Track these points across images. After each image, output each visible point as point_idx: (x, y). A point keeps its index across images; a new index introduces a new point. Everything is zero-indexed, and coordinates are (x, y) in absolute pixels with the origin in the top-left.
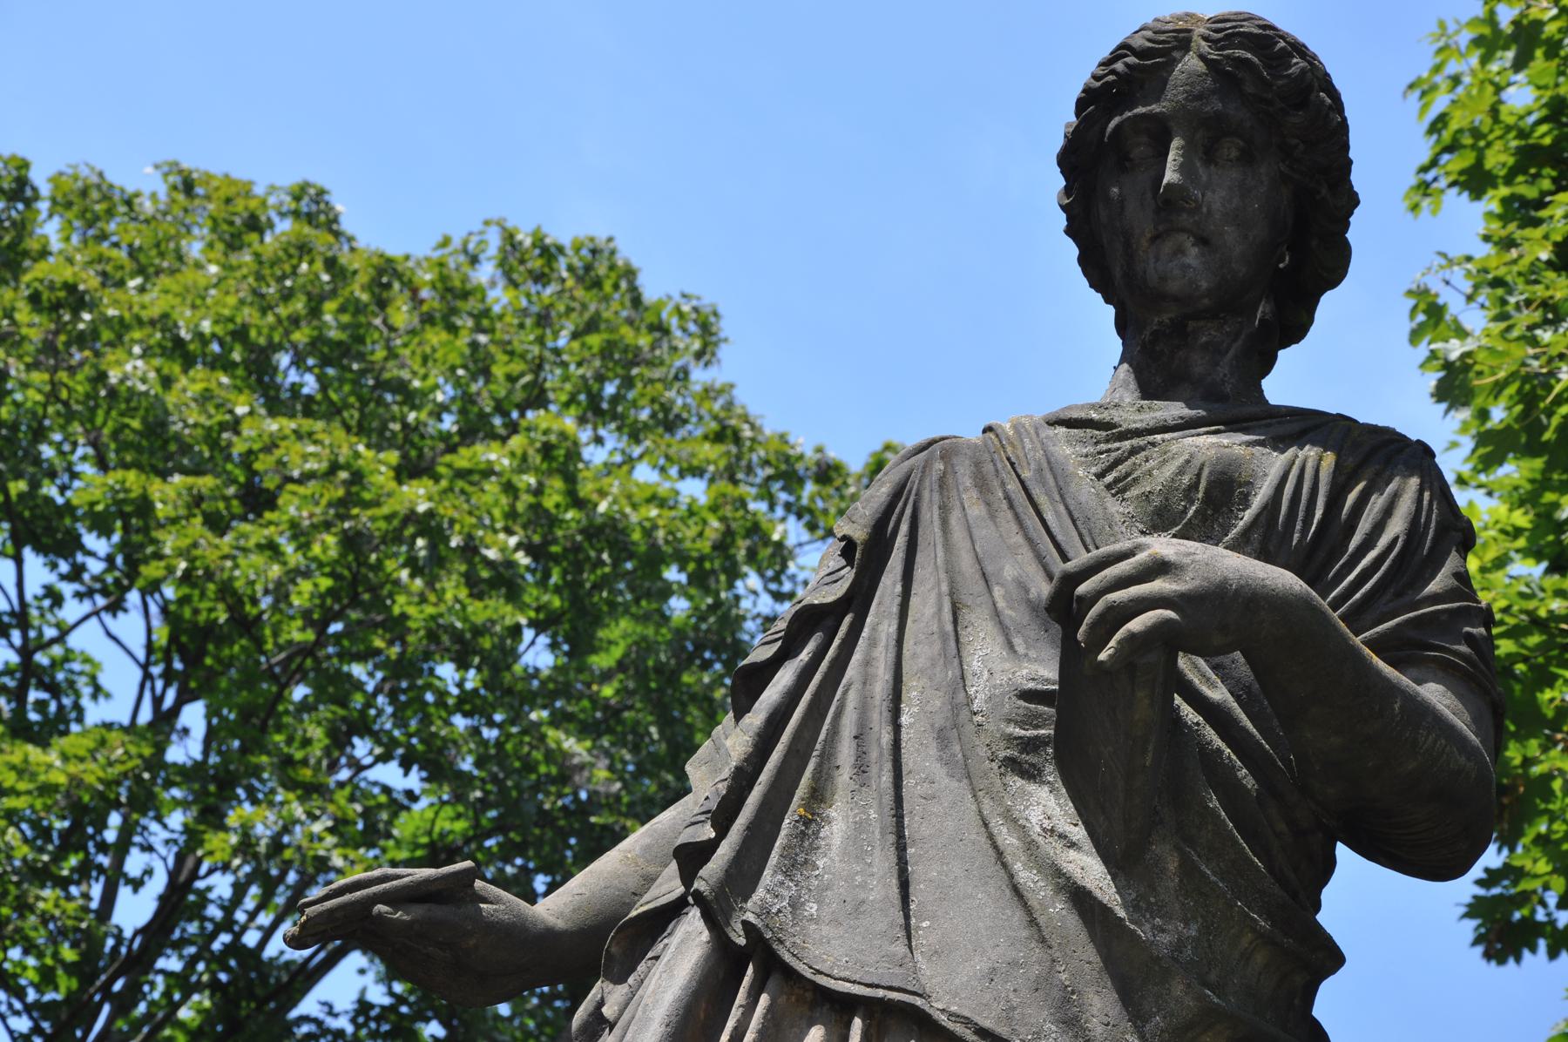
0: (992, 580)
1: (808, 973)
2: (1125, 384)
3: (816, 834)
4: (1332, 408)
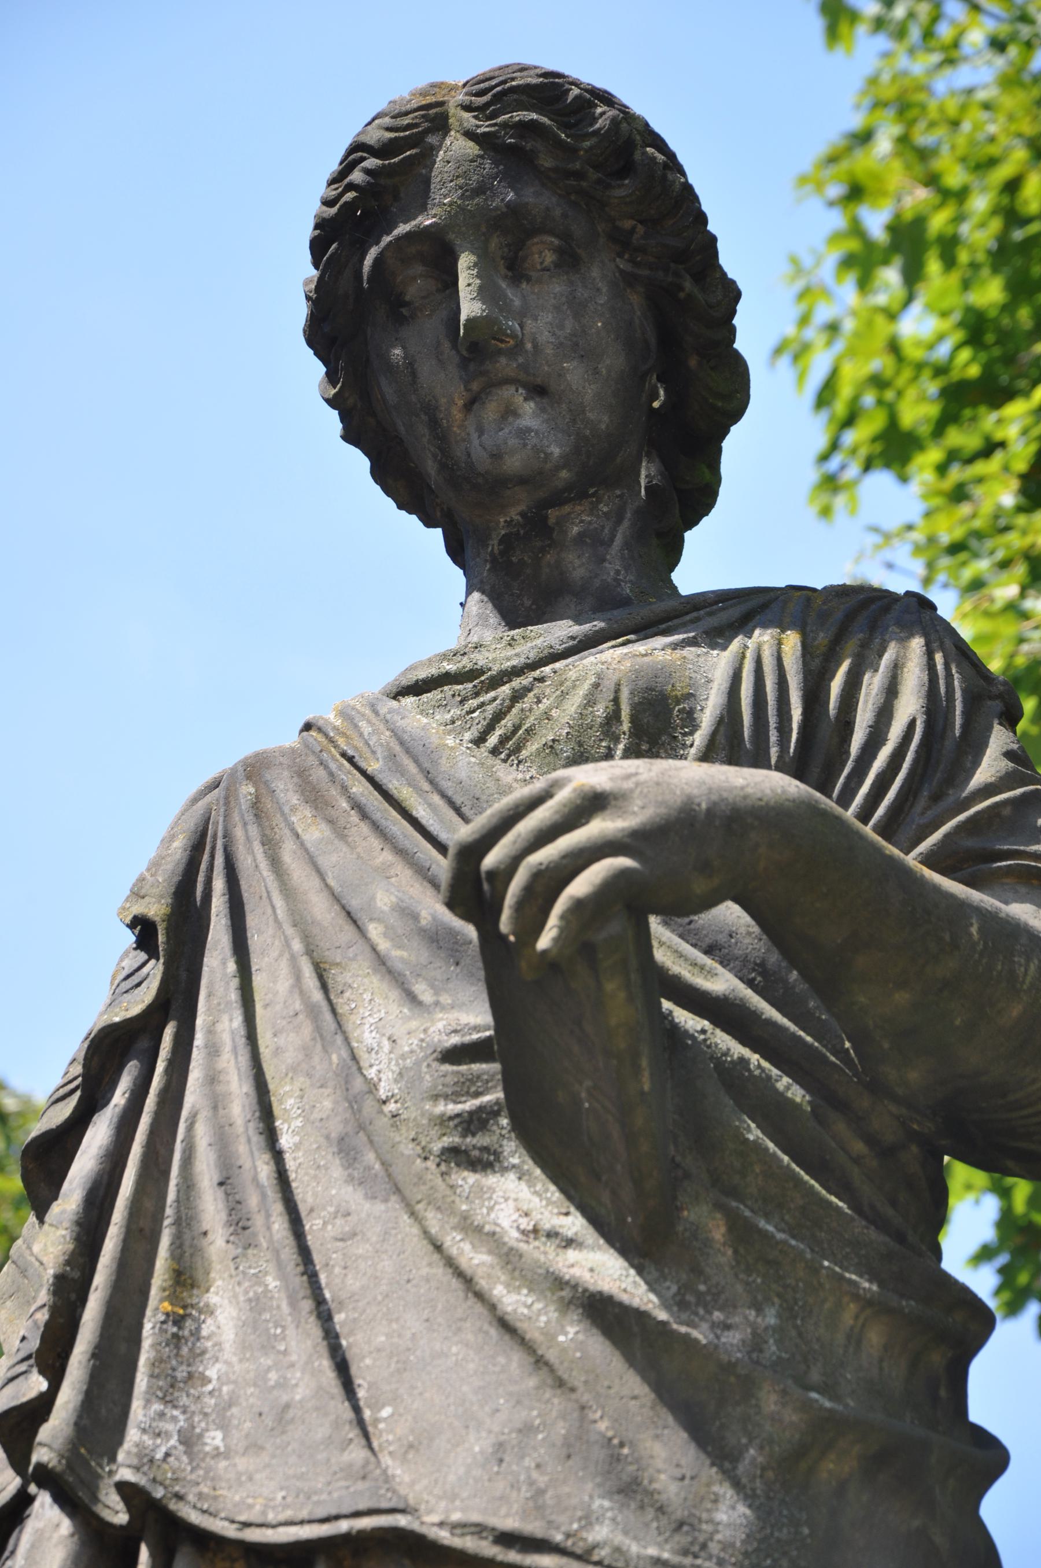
0: (362, 918)
1: (231, 1532)
2: (482, 621)
3: (196, 1334)
4: (779, 581)
